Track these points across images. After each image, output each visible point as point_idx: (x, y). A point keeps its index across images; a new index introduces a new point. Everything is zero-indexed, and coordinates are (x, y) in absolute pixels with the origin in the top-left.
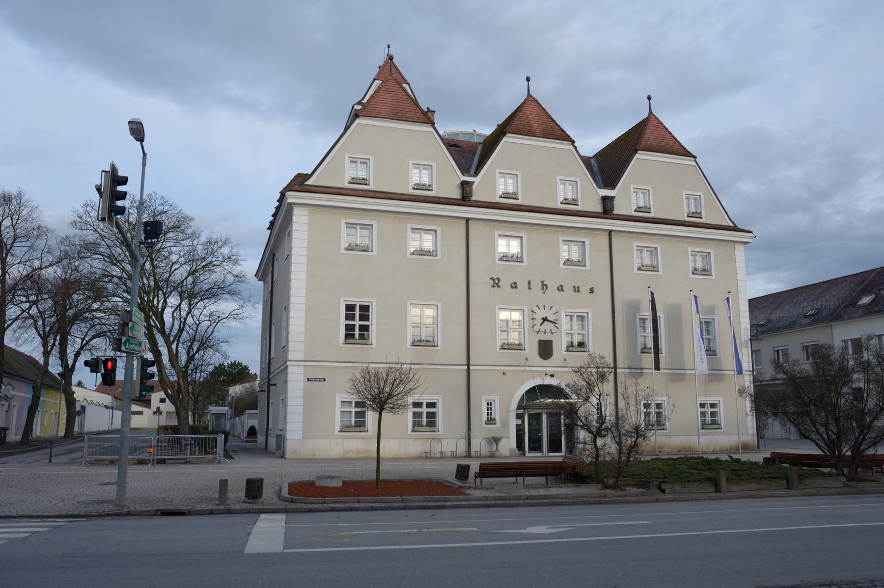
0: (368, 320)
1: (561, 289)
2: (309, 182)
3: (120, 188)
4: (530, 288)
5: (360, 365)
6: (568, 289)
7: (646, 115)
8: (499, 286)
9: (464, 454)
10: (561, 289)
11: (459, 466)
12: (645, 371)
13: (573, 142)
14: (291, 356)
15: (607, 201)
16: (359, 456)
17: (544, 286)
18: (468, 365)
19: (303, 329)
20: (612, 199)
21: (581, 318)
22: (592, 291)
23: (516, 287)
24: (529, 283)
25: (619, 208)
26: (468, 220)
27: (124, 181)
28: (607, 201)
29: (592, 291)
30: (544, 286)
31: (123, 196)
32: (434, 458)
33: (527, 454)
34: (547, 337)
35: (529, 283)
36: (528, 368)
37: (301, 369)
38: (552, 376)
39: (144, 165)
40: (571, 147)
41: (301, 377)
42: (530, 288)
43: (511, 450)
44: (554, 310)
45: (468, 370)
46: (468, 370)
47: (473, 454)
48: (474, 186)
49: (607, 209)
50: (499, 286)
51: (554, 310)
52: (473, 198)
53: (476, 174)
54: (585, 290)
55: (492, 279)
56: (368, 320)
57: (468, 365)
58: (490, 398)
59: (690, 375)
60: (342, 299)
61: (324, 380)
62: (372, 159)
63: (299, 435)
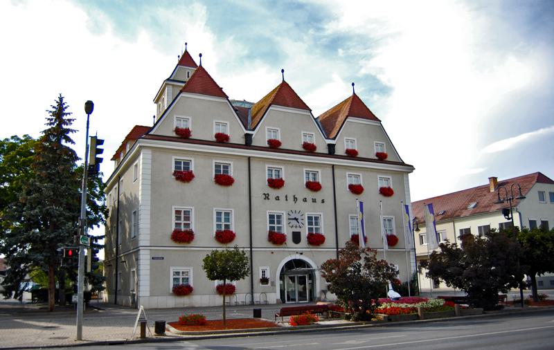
0: (189, 220)
1: (305, 200)
2: (151, 133)
3: (99, 147)
4: (287, 200)
5: (211, 249)
6: (310, 200)
7: (281, 82)
8: (268, 199)
9: (249, 303)
10: (305, 200)
11: (254, 310)
12: (140, 248)
13: (311, 111)
14: (141, 243)
15: (248, 137)
16: (185, 306)
17: (295, 199)
18: (251, 248)
19: (149, 226)
20: (334, 145)
21: (389, 220)
22: (323, 201)
23: (315, 202)
24: (286, 197)
25: (340, 151)
26: (249, 158)
27: (101, 142)
28: (248, 137)
29: (323, 201)
30: (295, 199)
31: (101, 151)
32: (232, 306)
33: (287, 302)
34: (297, 230)
35: (286, 197)
36: (286, 249)
37: (148, 252)
38: (301, 254)
39: (88, 128)
40: (310, 114)
41: (148, 257)
42: (287, 200)
43: (277, 300)
44: (301, 214)
45: (251, 250)
46: (251, 250)
47: (255, 303)
48: (253, 136)
49: (248, 143)
50: (268, 199)
51: (301, 214)
52: (336, 154)
53: (254, 130)
54: (319, 201)
55: (264, 194)
56: (189, 220)
57: (251, 248)
58: (264, 268)
59: (379, 252)
60: (214, 209)
61: (163, 258)
62: (190, 118)
63: (148, 294)
